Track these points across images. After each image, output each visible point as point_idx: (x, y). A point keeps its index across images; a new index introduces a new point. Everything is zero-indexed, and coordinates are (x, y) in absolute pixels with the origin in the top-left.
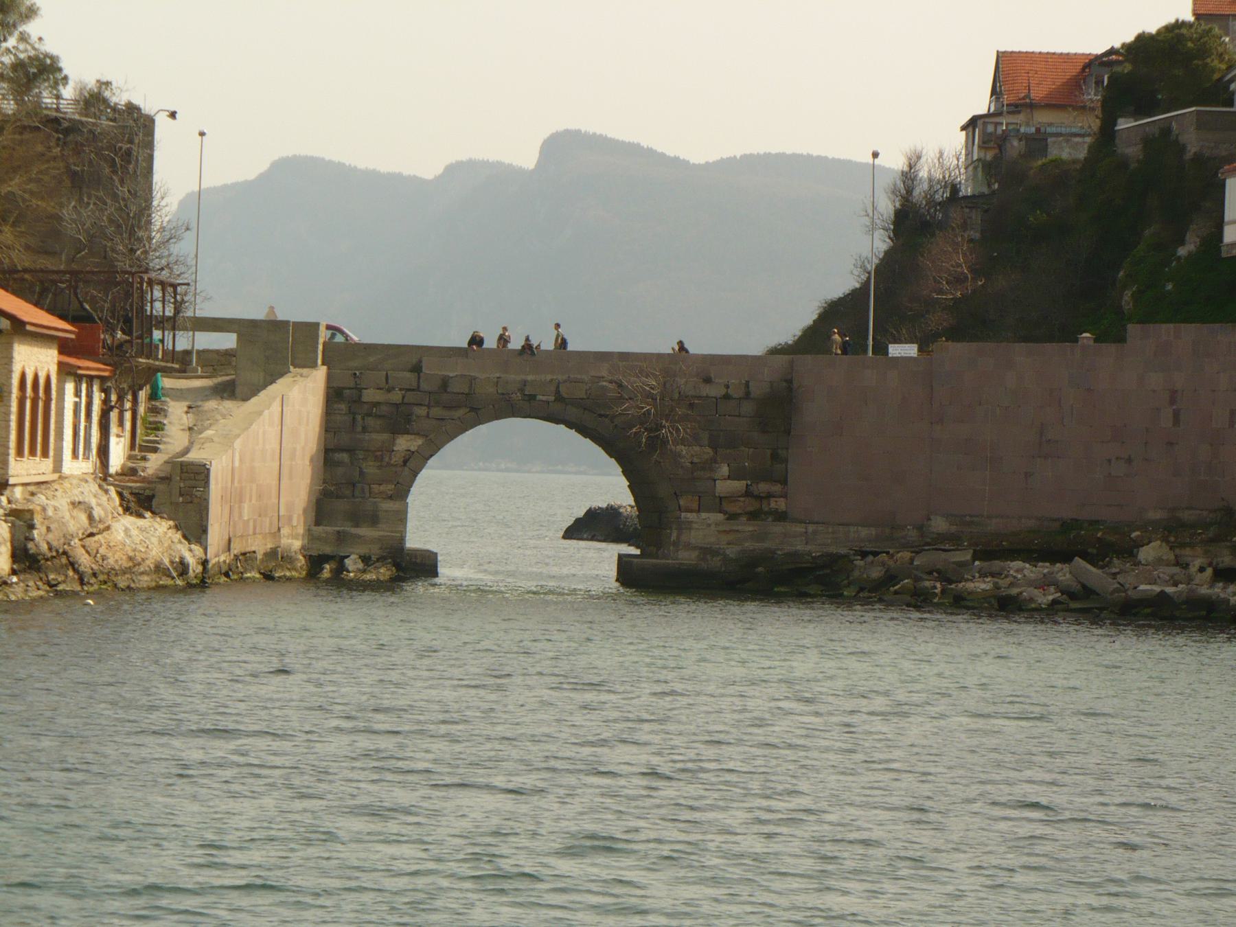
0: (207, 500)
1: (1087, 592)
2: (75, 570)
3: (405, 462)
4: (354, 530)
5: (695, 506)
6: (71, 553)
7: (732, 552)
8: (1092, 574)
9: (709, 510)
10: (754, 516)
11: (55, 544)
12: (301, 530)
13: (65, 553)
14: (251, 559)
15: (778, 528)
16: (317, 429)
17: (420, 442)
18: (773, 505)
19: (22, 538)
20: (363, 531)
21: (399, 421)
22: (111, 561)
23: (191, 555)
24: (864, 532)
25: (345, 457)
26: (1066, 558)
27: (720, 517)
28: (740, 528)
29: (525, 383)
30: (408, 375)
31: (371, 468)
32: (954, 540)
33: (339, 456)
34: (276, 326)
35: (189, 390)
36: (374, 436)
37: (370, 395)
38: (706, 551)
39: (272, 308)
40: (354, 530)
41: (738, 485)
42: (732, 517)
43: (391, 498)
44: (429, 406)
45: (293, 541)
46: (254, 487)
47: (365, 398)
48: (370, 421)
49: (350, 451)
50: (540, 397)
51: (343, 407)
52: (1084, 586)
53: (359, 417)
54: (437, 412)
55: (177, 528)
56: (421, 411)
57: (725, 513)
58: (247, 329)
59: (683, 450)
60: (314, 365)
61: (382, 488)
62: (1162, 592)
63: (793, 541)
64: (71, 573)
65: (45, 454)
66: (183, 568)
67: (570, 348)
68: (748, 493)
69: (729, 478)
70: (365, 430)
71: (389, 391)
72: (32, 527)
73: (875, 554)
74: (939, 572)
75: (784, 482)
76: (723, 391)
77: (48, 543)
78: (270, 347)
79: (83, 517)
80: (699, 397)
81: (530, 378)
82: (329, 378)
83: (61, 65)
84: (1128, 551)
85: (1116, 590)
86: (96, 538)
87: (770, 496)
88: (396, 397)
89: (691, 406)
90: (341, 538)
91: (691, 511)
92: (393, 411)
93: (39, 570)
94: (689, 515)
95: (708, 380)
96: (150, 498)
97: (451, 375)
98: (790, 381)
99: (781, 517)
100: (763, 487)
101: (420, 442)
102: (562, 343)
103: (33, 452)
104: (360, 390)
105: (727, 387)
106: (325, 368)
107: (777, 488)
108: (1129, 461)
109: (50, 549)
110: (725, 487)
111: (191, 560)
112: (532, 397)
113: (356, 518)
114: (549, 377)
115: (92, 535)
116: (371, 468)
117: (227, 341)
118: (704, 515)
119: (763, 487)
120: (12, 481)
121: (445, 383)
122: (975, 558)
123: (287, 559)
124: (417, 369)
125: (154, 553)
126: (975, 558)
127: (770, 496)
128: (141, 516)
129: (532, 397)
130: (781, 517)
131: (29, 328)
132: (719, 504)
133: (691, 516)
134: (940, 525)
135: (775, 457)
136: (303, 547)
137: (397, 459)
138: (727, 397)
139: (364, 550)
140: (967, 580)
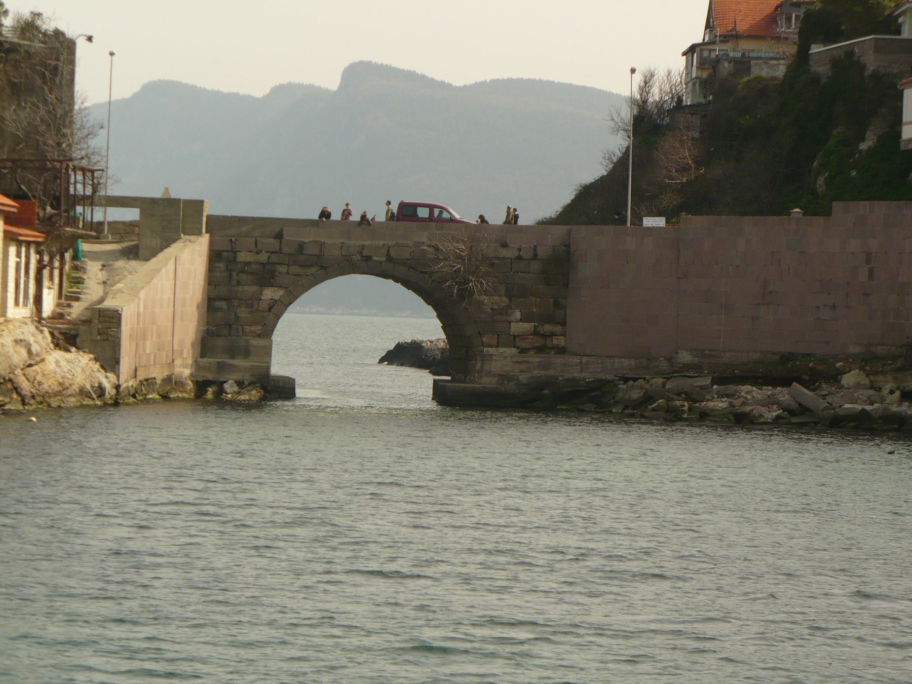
0: (119, 339)
1: (803, 409)
2: (19, 394)
3: (270, 309)
4: (231, 361)
5: (495, 342)
6: (15, 380)
7: (524, 378)
8: (807, 395)
9: (505, 346)
10: (540, 350)
13: (10, 380)
15: (559, 360)
16: (202, 283)
17: (281, 292)
18: (555, 342)
20: (239, 362)
21: (265, 276)
23: (107, 381)
24: (626, 362)
25: (223, 304)
26: (785, 382)
27: (514, 351)
29: (363, 247)
30: (272, 240)
31: (243, 313)
32: (696, 369)
33: (218, 304)
36: (246, 288)
37: (243, 256)
39: (167, 189)
40: (231, 361)
41: (528, 327)
42: (523, 351)
43: (259, 336)
44: (289, 265)
47: (238, 259)
48: (244, 277)
49: (228, 300)
50: (375, 258)
51: (222, 265)
52: (800, 405)
53: (234, 274)
54: (295, 269)
56: (284, 269)
57: (518, 348)
58: (147, 205)
59: (485, 299)
60: (199, 233)
61: (253, 328)
63: (571, 369)
64: (15, 396)
68: (535, 333)
69: (521, 320)
70: (238, 283)
71: (258, 253)
74: (686, 393)
75: (564, 324)
76: (516, 254)
78: (166, 219)
79: (24, 352)
81: (367, 243)
85: (826, 408)
87: (552, 335)
88: (263, 257)
90: (221, 367)
94: (490, 349)
95: (504, 245)
96: (75, 337)
98: (568, 246)
99: (561, 351)
100: (548, 328)
104: (235, 253)
105: (520, 250)
106: (208, 235)
107: (558, 329)
110: (519, 327)
111: (107, 385)
113: (233, 352)
114: (381, 243)
116: (243, 313)
117: (131, 214)
118: (501, 350)
119: (548, 328)
121: (301, 247)
124: (279, 236)
127: (552, 335)
128: (68, 351)
130: (561, 351)
132: (513, 340)
134: (685, 357)
135: (556, 304)
136: (191, 375)
137: (263, 306)
138: (519, 258)
139: (238, 377)
140: (708, 400)
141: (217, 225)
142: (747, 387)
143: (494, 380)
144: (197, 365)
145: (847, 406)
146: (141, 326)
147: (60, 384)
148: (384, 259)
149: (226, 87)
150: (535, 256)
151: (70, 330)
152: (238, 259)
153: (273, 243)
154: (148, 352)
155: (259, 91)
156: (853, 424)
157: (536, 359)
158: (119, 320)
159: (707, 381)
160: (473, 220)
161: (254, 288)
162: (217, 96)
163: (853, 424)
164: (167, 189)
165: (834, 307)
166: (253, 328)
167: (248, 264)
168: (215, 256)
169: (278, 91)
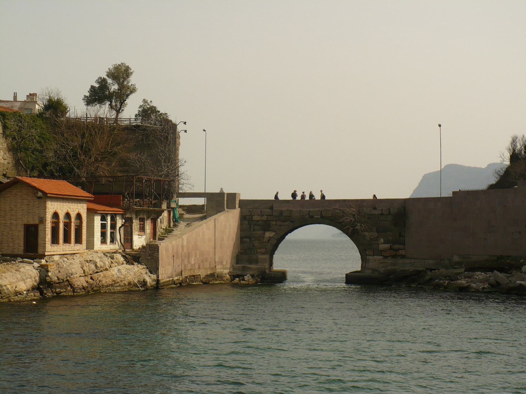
0: (158, 258)
1: (498, 284)
2: (72, 287)
3: (269, 241)
4: (248, 266)
5: (372, 254)
6: (70, 280)
7: (382, 270)
8: (501, 276)
9: (377, 255)
10: (394, 257)
11: (60, 277)
12: (228, 266)
13: (67, 280)
14: (197, 278)
15: (401, 261)
16: (236, 230)
17: (274, 234)
18: (400, 253)
19: (44, 276)
20: (253, 266)
21: (266, 226)
22: (103, 282)
23: (150, 279)
24: (431, 261)
25: (248, 240)
26: (491, 270)
27: (381, 257)
28: (387, 261)
29: (310, 211)
30: (268, 210)
31: (256, 243)
32: (460, 264)
33: (245, 240)
34: (221, 194)
35: (198, 217)
36: (258, 232)
37: (256, 218)
38: (374, 270)
39: (222, 189)
40: (248, 266)
41: (387, 246)
42: (386, 257)
43: (264, 254)
44: (276, 221)
45: (224, 268)
46: (198, 252)
47: (254, 219)
48: (256, 227)
49: (249, 238)
50: (315, 217)
51: (246, 222)
52: (497, 282)
53: (252, 226)
54: (279, 223)
55: (147, 268)
56: (274, 223)
57: (383, 256)
58: (210, 196)
59: (367, 234)
60: (234, 208)
61: (261, 250)
62: (521, 284)
63: (406, 266)
64: (69, 288)
65: (78, 240)
66: (144, 283)
67: (326, 199)
68: (391, 249)
69: (384, 243)
70: (254, 230)
71: (262, 216)
72: (48, 271)
73: (435, 270)
74: (449, 277)
75: (404, 244)
76: (380, 212)
77: (57, 277)
78: (218, 202)
79: (93, 266)
80: (372, 215)
81: (311, 210)
82: (241, 212)
83: (158, 109)
84: (518, 268)
85: (508, 283)
86: (99, 274)
87: (399, 249)
88: (265, 218)
89: (369, 218)
90: (244, 268)
91: (370, 256)
92: (266, 224)
93: (51, 288)
94: (369, 257)
95: (375, 208)
96: (139, 258)
97: (284, 209)
98: (405, 208)
99: (403, 257)
100: (396, 246)
101: (274, 234)
102: (323, 197)
103: (67, 240)
104: (252, 216)
105: (382, 210)
106: (239, 209)
107: (401, 247)
108: (520, 232)
109: (58, 279)
110: (382, 246)
111: (148, 280)
112: (312, 217)
113: (250, 262)
114: (318, 209)
115: (97, 272)
116: (256, 243)
117: (201, 201)
118: (375, 257)
119: (396, 246)
120: (46, 254)
121: (281, 213)
122: (465, 271)
123: (220, 277)
124: (272, 208)
125: (129, 278)
126: (465, 271)
127: (399, 249)
128: (133, 264)
129: (312, 217)
130: (403, 257)
131: (49, 195)
132: (381, 253)
133: (371, 258)
134: (456, 258)
135: (400, 235)
136: (230, 272)
137: (265, 240)
138: (382, 214)
139: (252, 273)
140: (459, 279)
141: (244, 204)
142: (479, 273)
143: (370, 271)
144: (232, 266)
145: (518, 282)
146: (185, 250)
147: (114, 281)
148: (319, 217)
149: (473, 165)
150: (390, 213)
151: (137, 254)
152: (254, 219)
153: (268, 211)
154: (193, 263)
155: (484, 166)
156: (515, 292)
157: (389, 261)
158: (158, 249)
159: (462, 270)
160: (371, 197)
161: (261, 232)
162: (470, 168)
163: (515, 292)
164: (222, 189)
165: (520, 232)
166: (261, 250)
167: (258, 221)
168: (243, 218)
169: (489, 165)
